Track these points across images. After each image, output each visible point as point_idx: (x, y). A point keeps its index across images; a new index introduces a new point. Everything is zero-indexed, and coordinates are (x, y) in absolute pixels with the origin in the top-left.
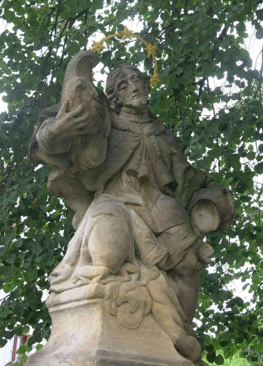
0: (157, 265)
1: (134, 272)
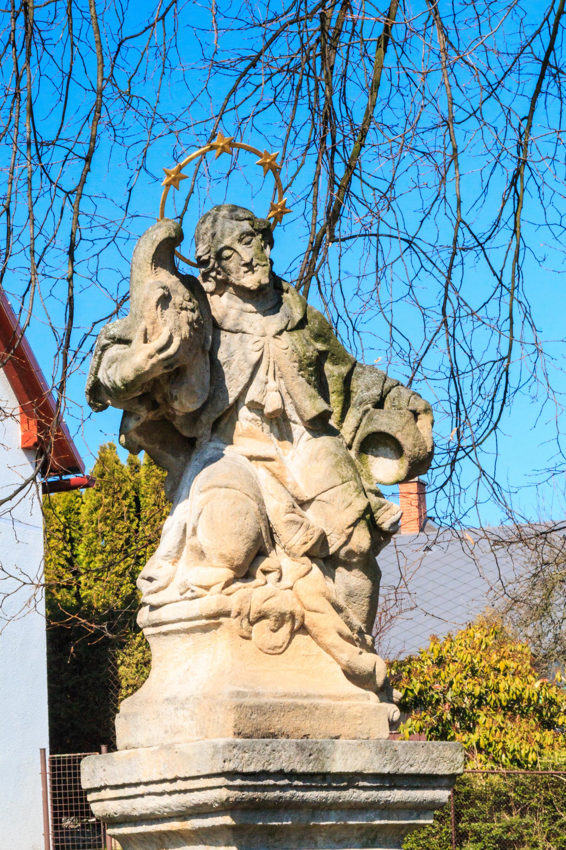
0: (306, 554)
1: (271, 570)
